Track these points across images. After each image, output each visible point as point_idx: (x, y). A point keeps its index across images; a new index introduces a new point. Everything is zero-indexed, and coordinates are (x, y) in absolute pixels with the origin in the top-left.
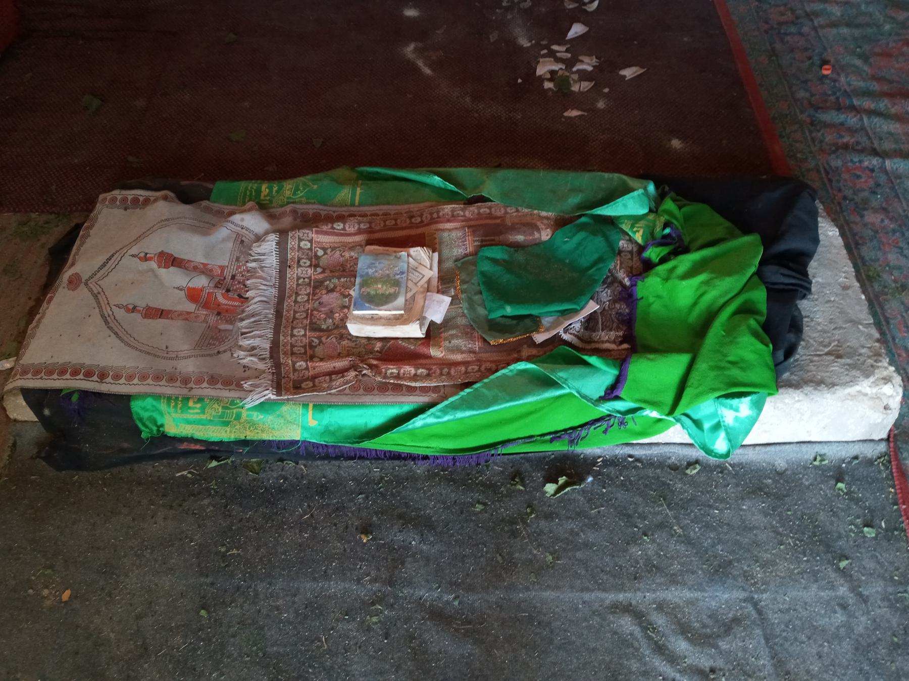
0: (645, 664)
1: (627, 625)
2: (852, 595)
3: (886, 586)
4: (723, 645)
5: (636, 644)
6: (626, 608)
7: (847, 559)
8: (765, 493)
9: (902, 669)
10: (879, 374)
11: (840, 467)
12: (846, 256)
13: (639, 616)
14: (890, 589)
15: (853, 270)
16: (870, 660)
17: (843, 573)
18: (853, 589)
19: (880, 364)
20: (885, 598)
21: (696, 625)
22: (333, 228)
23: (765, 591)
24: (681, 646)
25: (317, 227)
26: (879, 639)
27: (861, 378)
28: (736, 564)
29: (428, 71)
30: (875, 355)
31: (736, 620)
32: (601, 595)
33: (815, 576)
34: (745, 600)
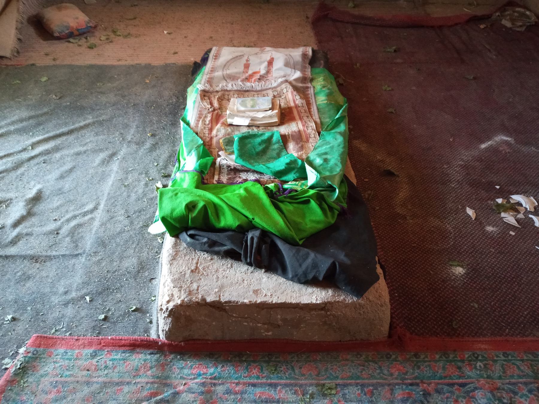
0: (71, 212)
1: (90, 207)
2: (70, 297)
3: (69, 318)
4: (68, 239)
5: (80, 210)
6: (96, 208)
7: (90, 301)
8: (140, 270)
9: (26, 313)
10: (176, 292)
11: (148, 313)
12: (289, 301)
13: (92, 211)
14: (67, 319)
15: (274, 302)
16: (37, 298)
17: (83, 297)
18: (73, 299)
19: (183, 292)
20: (63, 316)
21: (80, 231)
22: (296, 96)
23: (86, 259)
24: (73, 223)
25: (294, 90)
26: (44, 306)
27: (172, 277)
28: (103, 249)
29: (483, 146)
30: (190, 291)
31: (77, 246)
32: (105, 198)
33: (86, 284)
34: (85, 251)
